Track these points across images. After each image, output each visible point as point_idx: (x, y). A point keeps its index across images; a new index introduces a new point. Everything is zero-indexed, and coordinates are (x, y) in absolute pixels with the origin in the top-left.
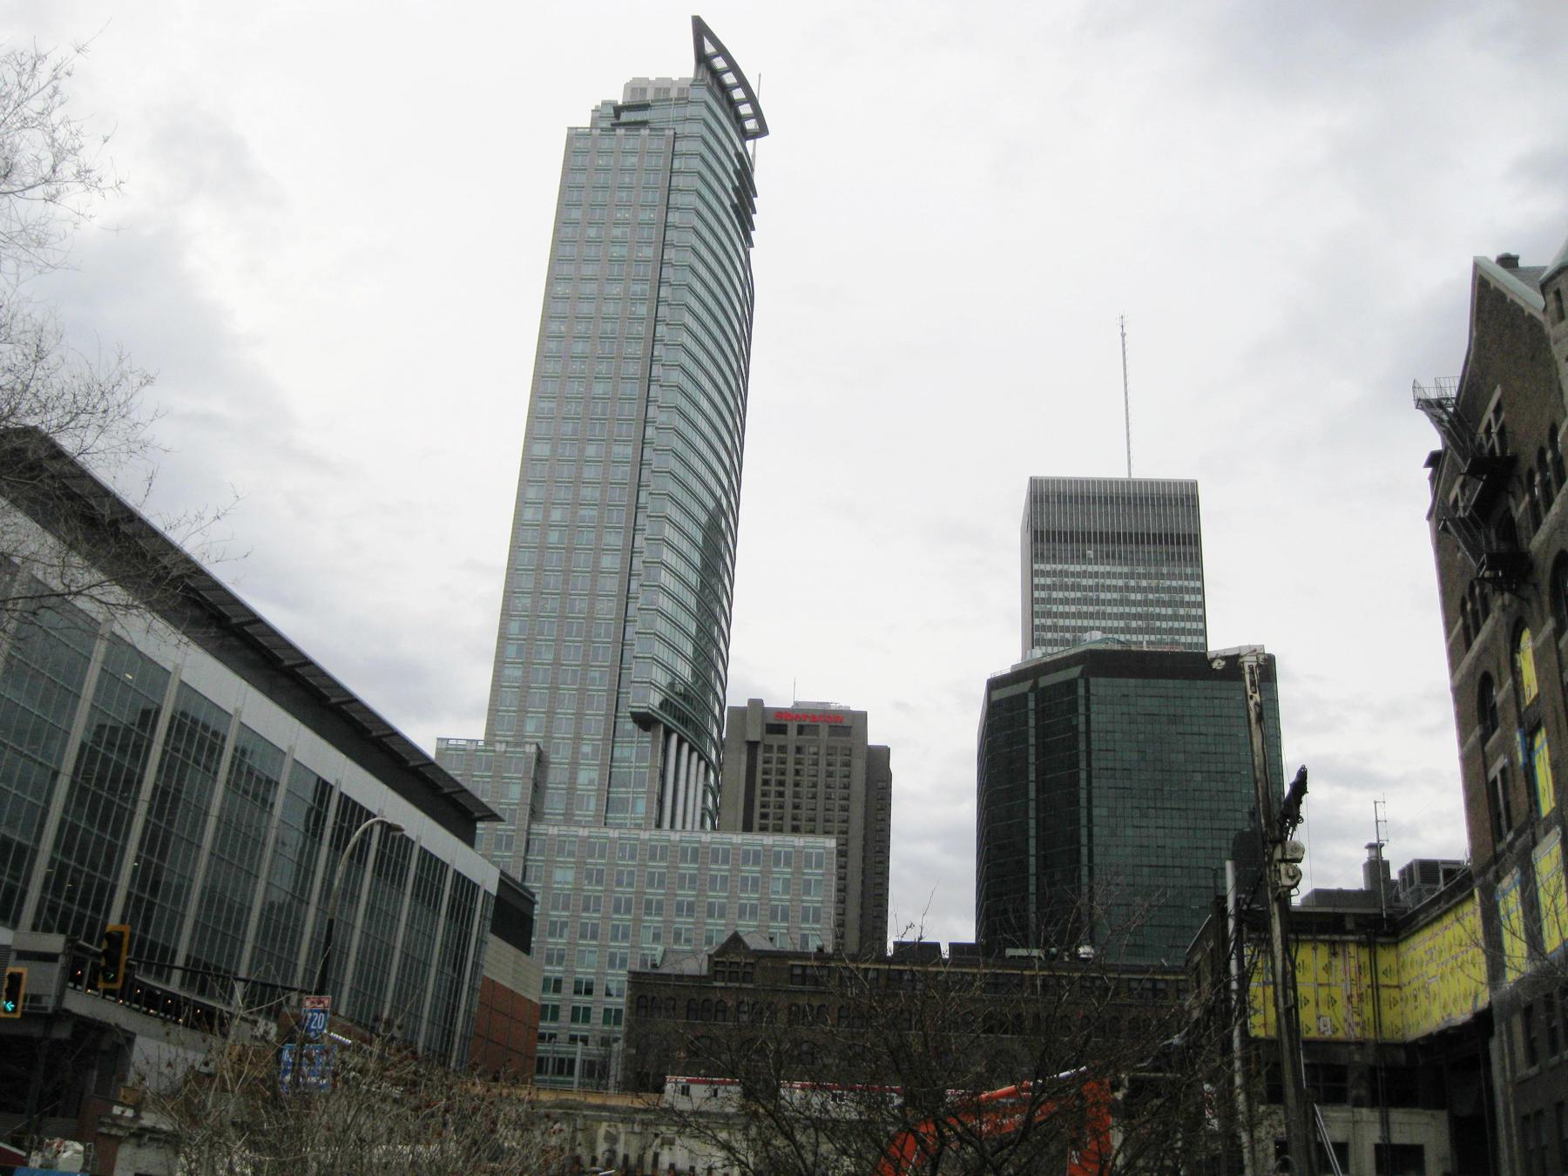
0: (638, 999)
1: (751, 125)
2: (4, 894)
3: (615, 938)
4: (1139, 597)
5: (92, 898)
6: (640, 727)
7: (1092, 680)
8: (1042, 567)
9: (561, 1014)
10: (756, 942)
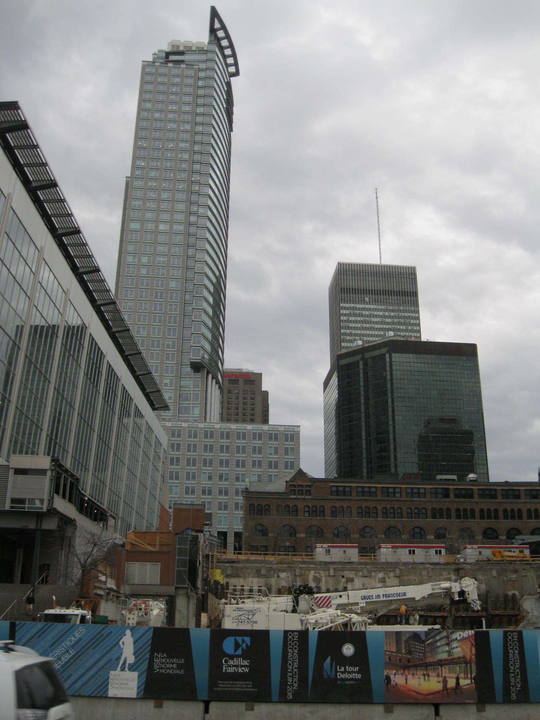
0: (250, 506)
3: (188, 479)
4: (390, 320)
7: (393, 355)
8: (344, 305)
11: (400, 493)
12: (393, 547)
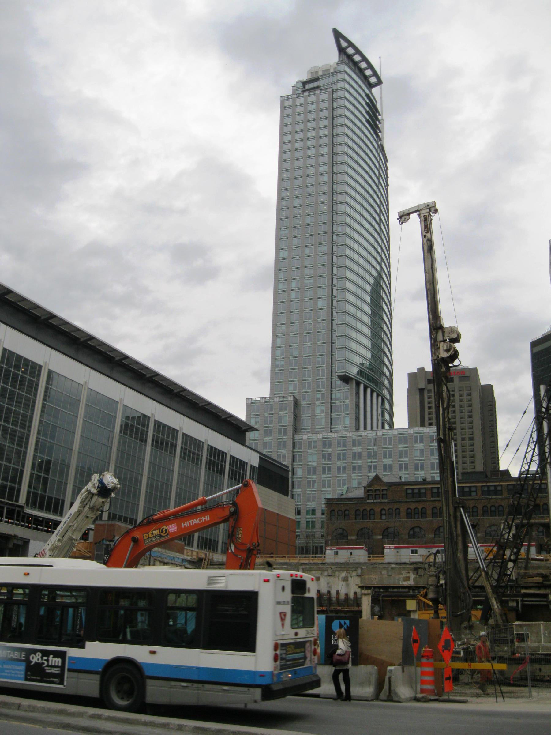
1: (373, 80)
6: (343, 382)
9: (301, 525)
10: (388, 477)
11: (476, 491)
12: (396, 548)
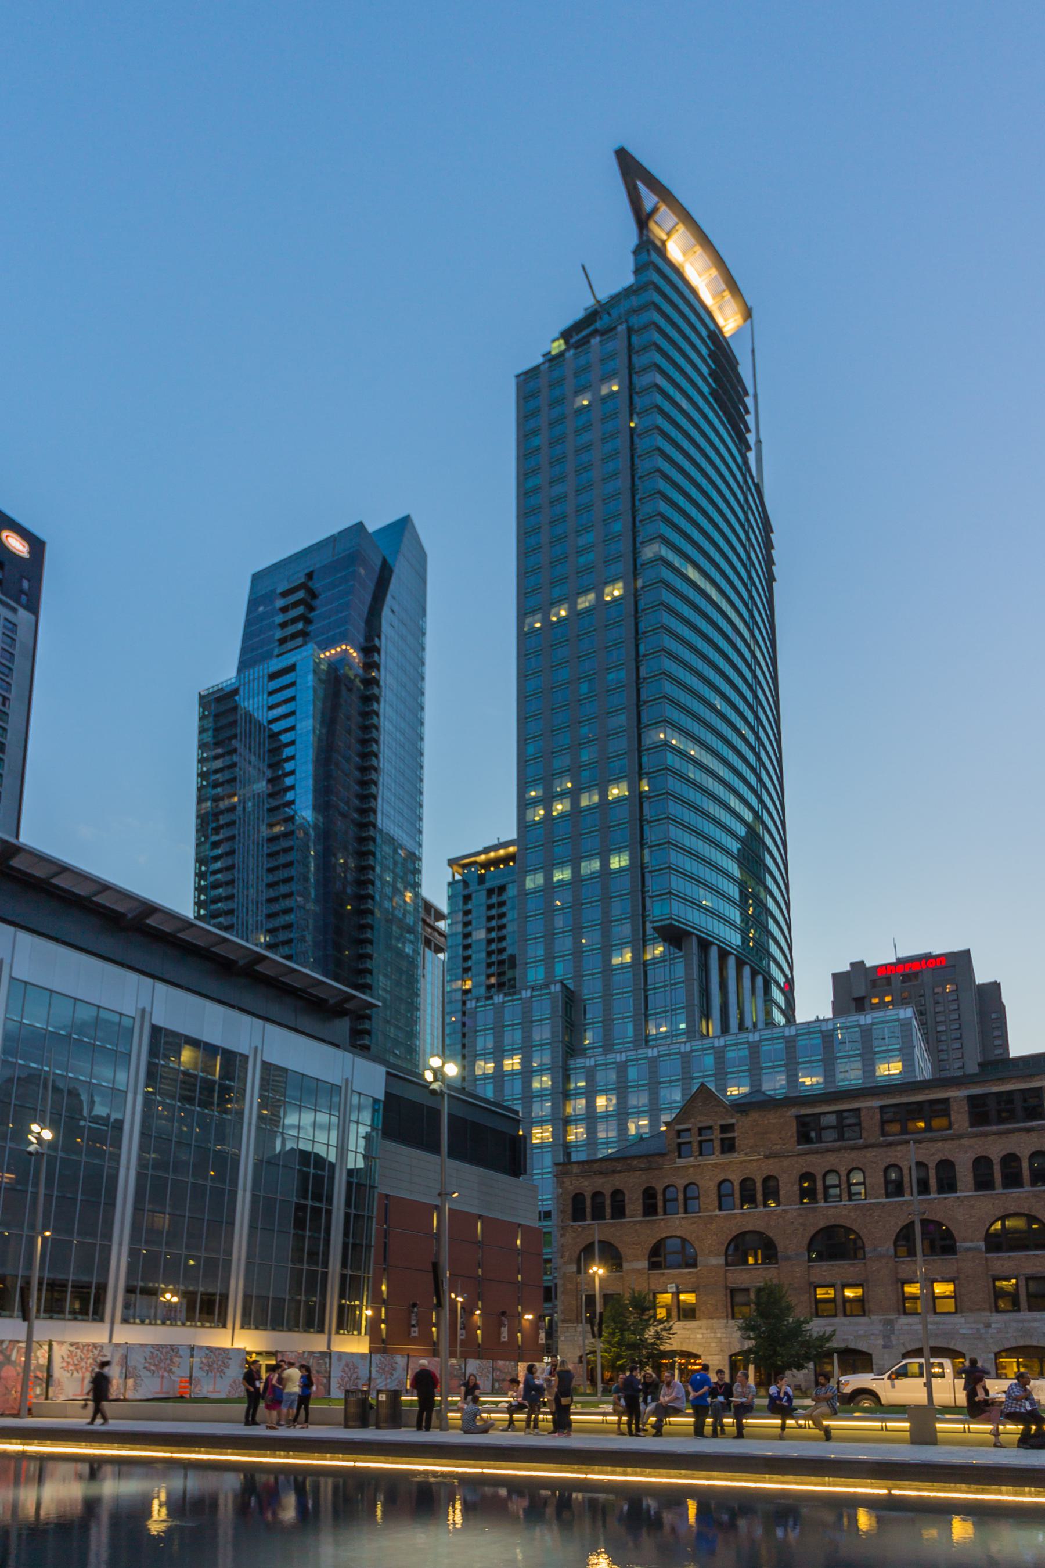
2: (4, 1201)
5: (78, 1209)
6: (670, 944)
